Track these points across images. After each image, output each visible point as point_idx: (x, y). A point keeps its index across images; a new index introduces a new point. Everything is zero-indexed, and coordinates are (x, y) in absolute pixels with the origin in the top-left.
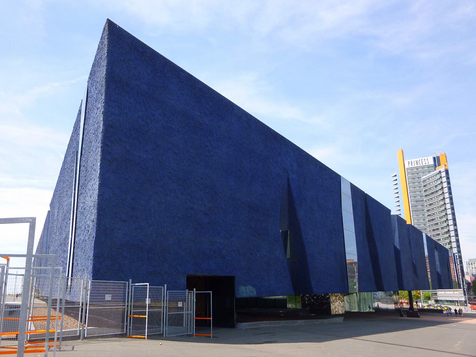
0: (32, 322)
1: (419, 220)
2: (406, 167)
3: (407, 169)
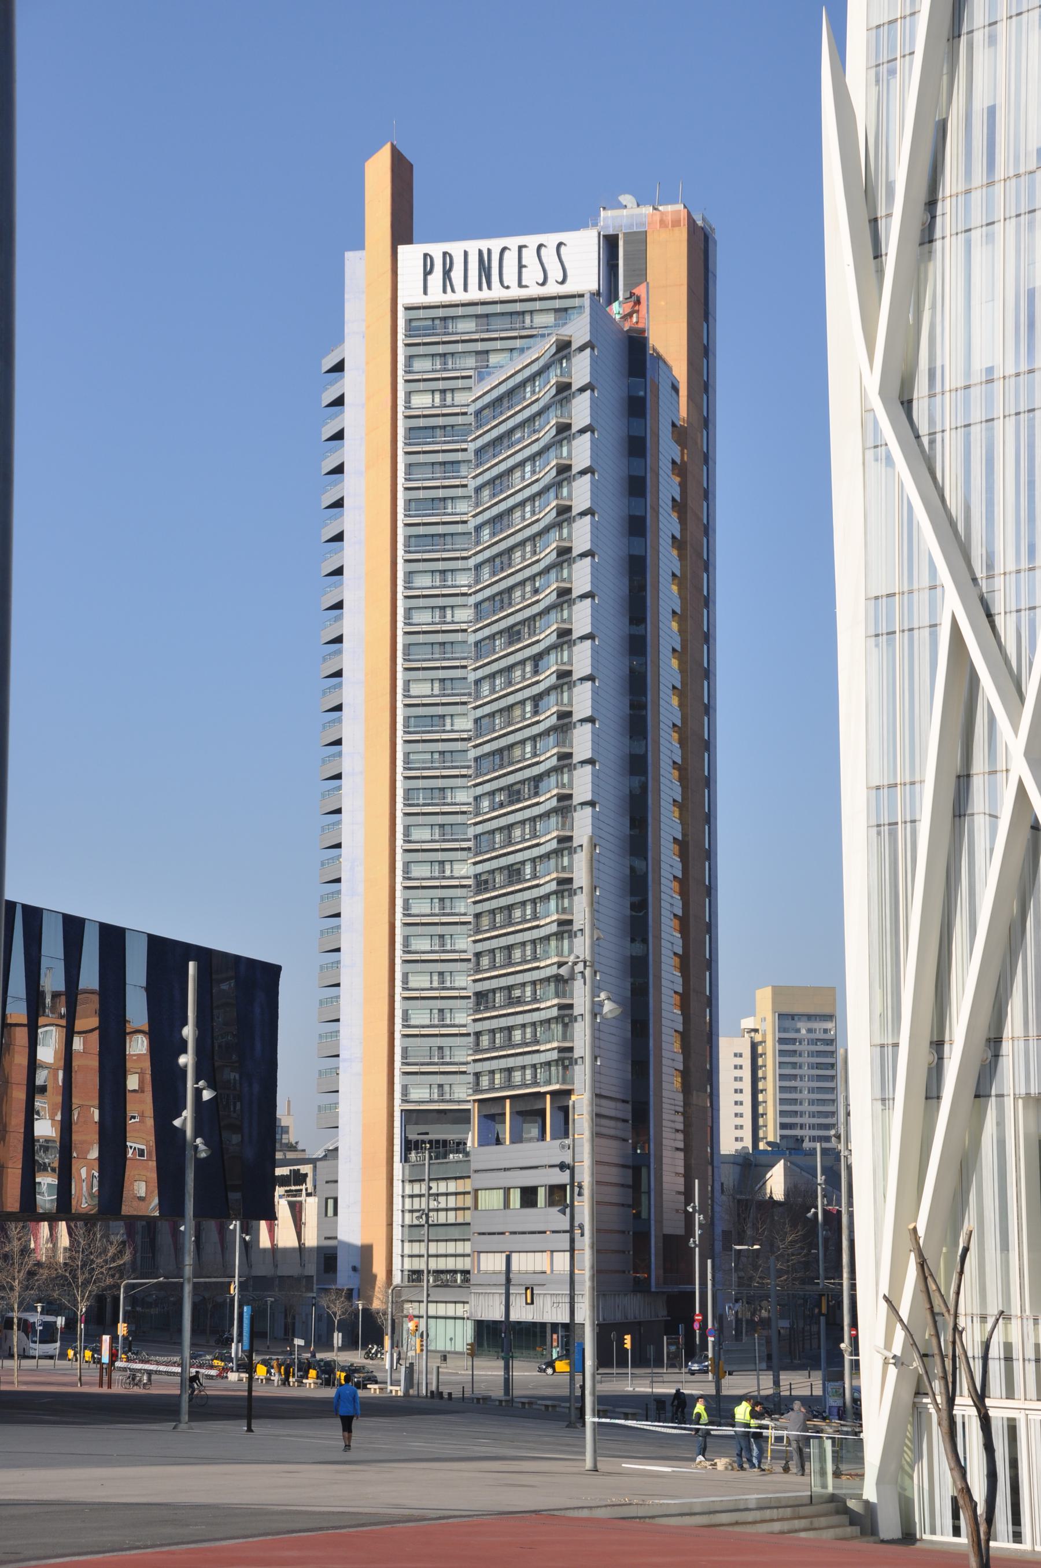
0: (62, 1226)
1: (448, 829)
2: (403, 300)
3: (414, 314)
